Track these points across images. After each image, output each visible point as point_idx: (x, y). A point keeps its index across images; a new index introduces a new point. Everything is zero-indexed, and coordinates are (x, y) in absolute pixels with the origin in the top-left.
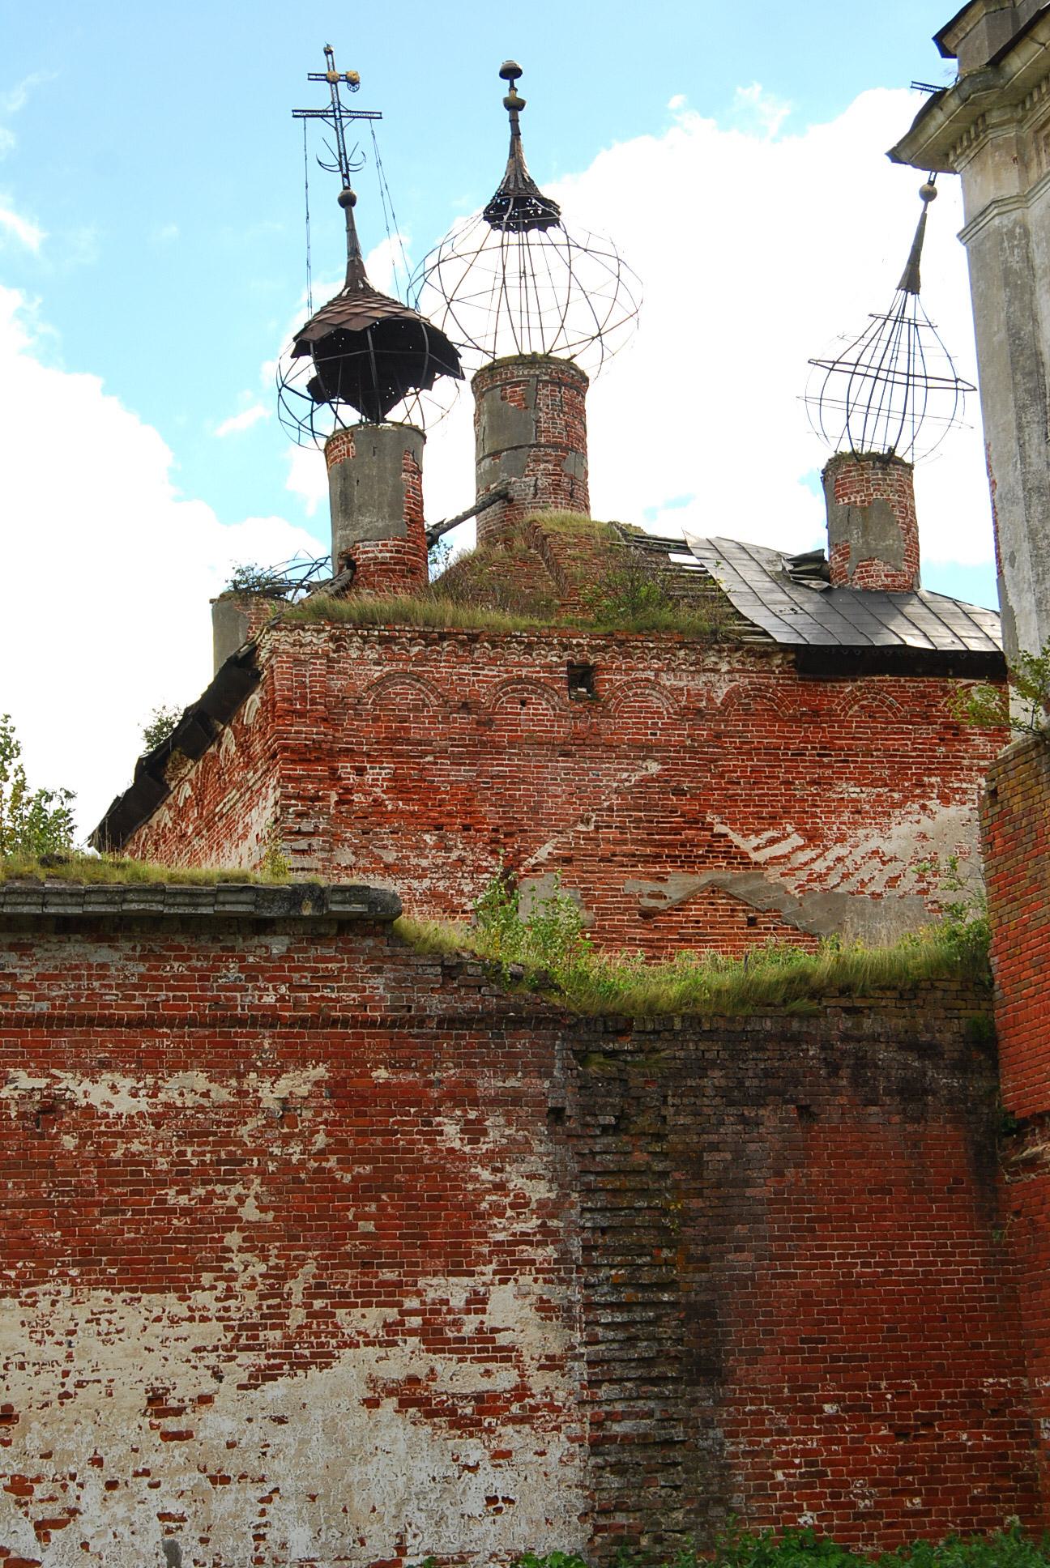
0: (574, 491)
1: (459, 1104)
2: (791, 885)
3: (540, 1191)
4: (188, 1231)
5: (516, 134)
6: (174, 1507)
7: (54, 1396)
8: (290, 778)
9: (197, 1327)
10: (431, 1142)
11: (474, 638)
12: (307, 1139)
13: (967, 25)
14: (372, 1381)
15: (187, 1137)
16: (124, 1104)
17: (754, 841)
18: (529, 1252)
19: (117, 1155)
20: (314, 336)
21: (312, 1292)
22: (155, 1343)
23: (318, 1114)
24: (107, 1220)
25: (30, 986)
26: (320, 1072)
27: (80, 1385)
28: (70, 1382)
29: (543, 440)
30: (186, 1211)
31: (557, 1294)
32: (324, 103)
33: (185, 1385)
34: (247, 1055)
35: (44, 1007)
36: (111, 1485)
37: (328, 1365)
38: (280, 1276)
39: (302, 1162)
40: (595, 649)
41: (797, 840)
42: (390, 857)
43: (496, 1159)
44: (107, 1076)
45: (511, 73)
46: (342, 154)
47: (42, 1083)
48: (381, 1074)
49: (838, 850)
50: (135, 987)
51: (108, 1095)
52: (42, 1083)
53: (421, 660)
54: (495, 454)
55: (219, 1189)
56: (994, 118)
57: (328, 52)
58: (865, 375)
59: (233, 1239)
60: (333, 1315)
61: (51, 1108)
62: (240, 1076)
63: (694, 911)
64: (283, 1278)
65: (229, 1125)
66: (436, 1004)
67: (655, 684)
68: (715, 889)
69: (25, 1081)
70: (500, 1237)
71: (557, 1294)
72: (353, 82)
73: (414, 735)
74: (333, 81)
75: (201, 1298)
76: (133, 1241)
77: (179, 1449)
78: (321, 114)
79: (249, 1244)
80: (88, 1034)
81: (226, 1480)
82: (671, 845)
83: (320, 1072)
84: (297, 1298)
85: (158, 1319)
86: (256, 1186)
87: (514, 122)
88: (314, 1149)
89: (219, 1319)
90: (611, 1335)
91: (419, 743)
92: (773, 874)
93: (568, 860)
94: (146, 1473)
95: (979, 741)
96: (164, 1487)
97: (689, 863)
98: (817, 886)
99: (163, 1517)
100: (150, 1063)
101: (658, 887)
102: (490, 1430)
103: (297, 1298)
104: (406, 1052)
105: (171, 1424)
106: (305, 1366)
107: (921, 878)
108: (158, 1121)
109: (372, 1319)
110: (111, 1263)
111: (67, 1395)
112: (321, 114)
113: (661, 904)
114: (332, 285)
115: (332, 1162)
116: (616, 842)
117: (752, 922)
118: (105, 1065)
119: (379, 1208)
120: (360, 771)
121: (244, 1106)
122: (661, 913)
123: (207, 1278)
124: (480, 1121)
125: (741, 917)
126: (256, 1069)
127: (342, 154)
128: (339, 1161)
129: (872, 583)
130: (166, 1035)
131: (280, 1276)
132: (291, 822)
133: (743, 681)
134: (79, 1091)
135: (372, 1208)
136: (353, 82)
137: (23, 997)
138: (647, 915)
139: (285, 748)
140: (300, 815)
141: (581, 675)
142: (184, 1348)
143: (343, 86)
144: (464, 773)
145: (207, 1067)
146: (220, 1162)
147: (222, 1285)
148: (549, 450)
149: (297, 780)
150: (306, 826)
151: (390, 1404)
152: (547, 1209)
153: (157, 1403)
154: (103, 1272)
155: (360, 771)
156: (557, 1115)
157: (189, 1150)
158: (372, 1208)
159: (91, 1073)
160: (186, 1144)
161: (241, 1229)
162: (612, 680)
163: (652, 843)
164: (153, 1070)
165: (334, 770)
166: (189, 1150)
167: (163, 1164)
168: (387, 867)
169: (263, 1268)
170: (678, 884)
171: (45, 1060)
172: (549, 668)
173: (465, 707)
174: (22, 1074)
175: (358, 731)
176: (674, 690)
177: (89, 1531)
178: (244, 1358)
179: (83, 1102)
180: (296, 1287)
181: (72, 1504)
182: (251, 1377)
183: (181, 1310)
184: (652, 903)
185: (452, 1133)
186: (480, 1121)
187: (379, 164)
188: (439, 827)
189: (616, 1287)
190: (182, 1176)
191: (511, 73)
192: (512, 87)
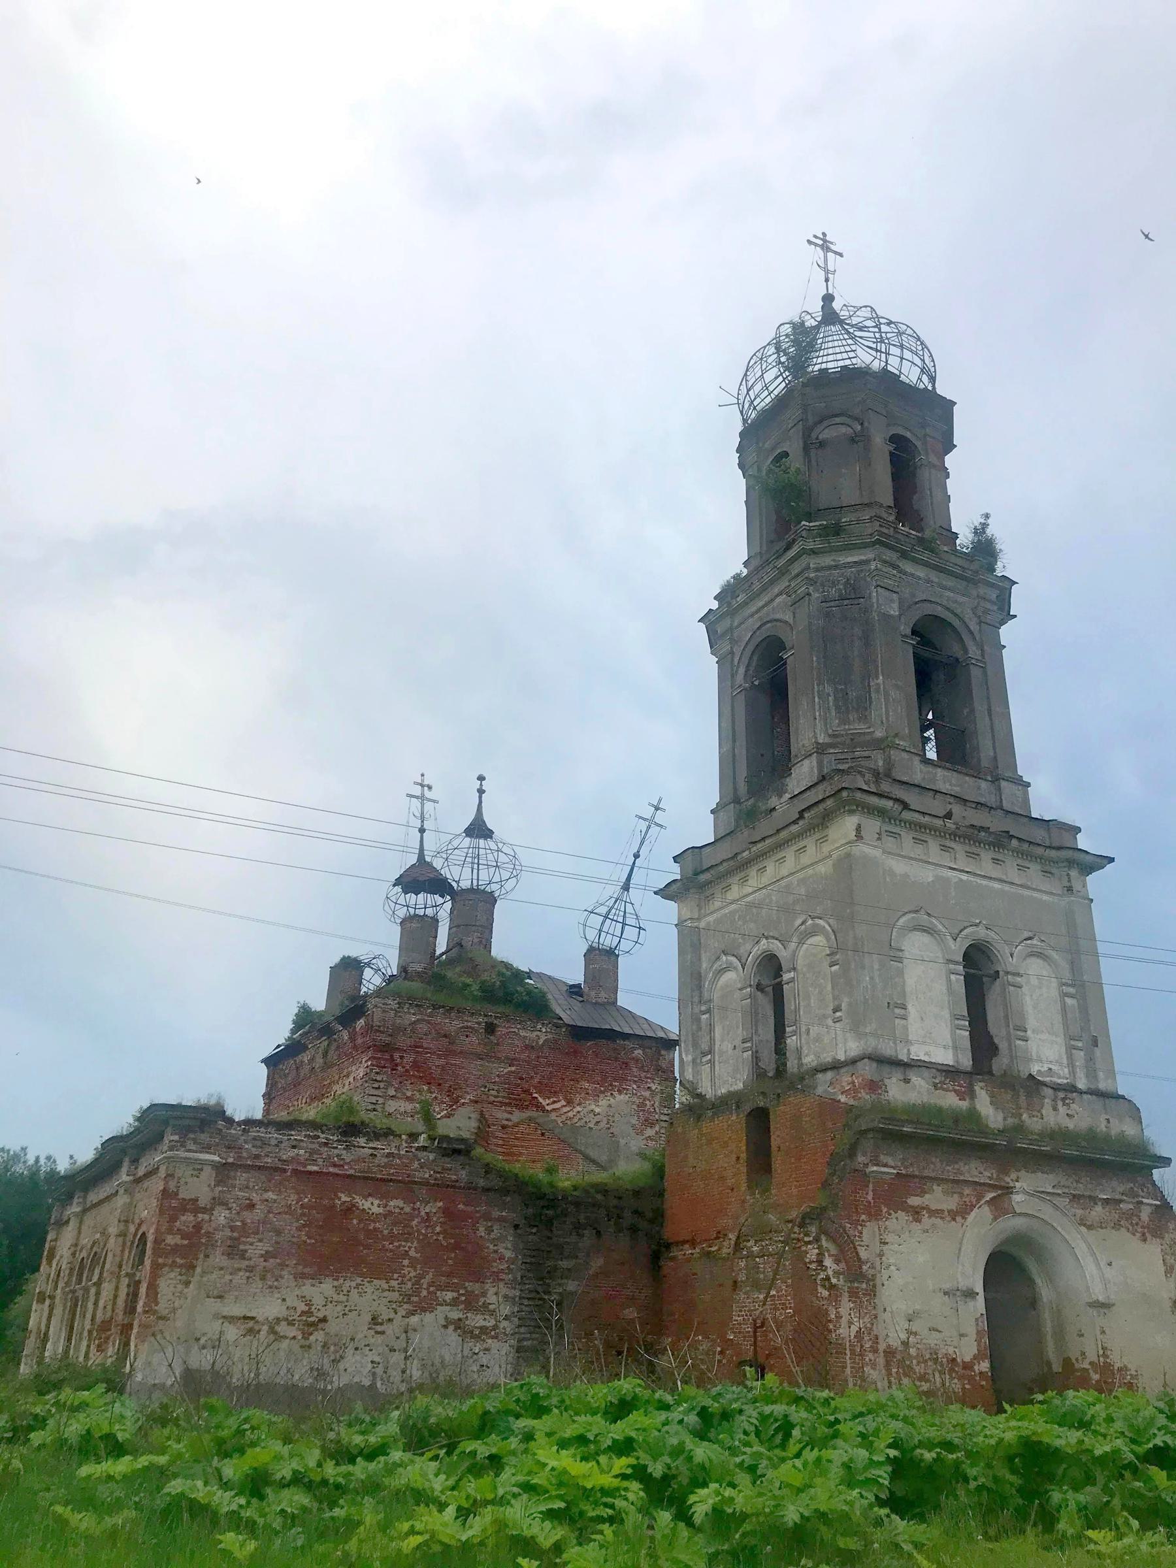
0: (488, 946)
1: (486, 1220)
2: (559, 1120)
3: (508, 1254)
5: (480, 802)
6: (377, 1359)
8: (374, 1058)
9: (390, 1293)
11: (452, 1008)
13: (685, 855)
14: (446, 1318)
15: (394, 1224)
16: (375, 1210)
17: (548, 1101)
18: (503, 1276)
19: (371, 1228)
20: (404, 880)
21: (430, 1285)
23: (439, 1218)
25: (348, 1163)
27: (350, 1311)
28: (347, 1309)
30: (391, 1251)
31: (511, 1293)
32: (418, 793)
33: (386, 1314)
35: (351, 1172)
36: (356, 1349)
38: (420, 1277)
40: (496, 1017)
41: (563, 1103)
42: (409, 1094)
43: (495, 1241)
44: (370, 1199)
45: (481, 778)
46: (422, 813)
48: (461, 1206)
49: (578, 1109)
50: (383, 1167)
51: (370, 1206)
52: (348, 1199)
54: (458, 926)
55: (403, 1243)
56: (691, 891)
57: (423, 775)
59: (406, 1262)
61: (350, 1209)
63: (521, 1128)
64: (421, 1278)
66: (482, 1183)
68: (530, 1119)
69: (344, 1198)
70: (495, 1270)
71: (511, 1293)
72: (430, 788)
73: (425, 1045)
74: (422, 786)
75: (394, 1283)
77: (380, 1338)
78: (417, 797)
79: (412, 1265)
81: (395, 1351)
82: (515, 1099)
84: (425, 1286)
86: (415, 1244)
87: (480, 797)
90: (527, 1309)
92: (553, 1116)
93: (476, 1102)
94: (368, 1345)
95: (635, 1070)
97: (521, 1107)
98: (569, 1122)
99: (372, 1362)
100: (385, 1197)
101: (509, 1116)
102: (484, 1340)
103: (425, 1286)
105: (379, 1328)
106: (425, 1311)
107: (608, 1123)
108: (385, 1216)
109: (449, 1296)
110: (365, 1267)
112: (417, 797)
113: (510, 1124)
114: (413, 859)
115: (441, 1237)
116: (496, 1097)
117: (543, 1134)
118: (370, 1195)
120: (402, 1057)
122: (509, 1127)
123: (396, 1276)
124: (491, 1226)
125: (539, 1132)
127: (422, 813)
129: (599, 1000)
131: (420, 1277)
132: (373, 1076)
133: (550, 1036)
135: (453, 1255)
136: (430, 788)
137: (346, 1167)
138: (504, 1127)
139: (375, 1046)
140: (377, 1073)
141: (490, 1029)
143: (426, 788)
144: (442, 1062)
150: (379, 1078)
151: (451, 1328)
152: (512, 1261)
153: (375, 1320)
155: (402, 1057)
156: (516, 1227)
158: (453, 1255)
159: (365, 1197)
162: (501, 1031)
163: (510, 1098)
165: (392, 1056)
167: (386, 1232)
168: (407, 1097)
169: (414, 1274)
170: (517, 1116)
172: (479, 1023)
173: (445, 1036)
174: (343, 1195)
175: (403, 1041)
176: (525, 1037)
177: (347, 1366)
178: (405, 1306)
179: (361, 1208)
183: (386, 1286)
184: (506, 1123)
185: (482, 1231)
186: (491, 1226)
187: (436, 819)
188: (429, 1084)
189: (530, 1291)
190: (392, 1238)
191: (481, 778)
192: (481, 785)
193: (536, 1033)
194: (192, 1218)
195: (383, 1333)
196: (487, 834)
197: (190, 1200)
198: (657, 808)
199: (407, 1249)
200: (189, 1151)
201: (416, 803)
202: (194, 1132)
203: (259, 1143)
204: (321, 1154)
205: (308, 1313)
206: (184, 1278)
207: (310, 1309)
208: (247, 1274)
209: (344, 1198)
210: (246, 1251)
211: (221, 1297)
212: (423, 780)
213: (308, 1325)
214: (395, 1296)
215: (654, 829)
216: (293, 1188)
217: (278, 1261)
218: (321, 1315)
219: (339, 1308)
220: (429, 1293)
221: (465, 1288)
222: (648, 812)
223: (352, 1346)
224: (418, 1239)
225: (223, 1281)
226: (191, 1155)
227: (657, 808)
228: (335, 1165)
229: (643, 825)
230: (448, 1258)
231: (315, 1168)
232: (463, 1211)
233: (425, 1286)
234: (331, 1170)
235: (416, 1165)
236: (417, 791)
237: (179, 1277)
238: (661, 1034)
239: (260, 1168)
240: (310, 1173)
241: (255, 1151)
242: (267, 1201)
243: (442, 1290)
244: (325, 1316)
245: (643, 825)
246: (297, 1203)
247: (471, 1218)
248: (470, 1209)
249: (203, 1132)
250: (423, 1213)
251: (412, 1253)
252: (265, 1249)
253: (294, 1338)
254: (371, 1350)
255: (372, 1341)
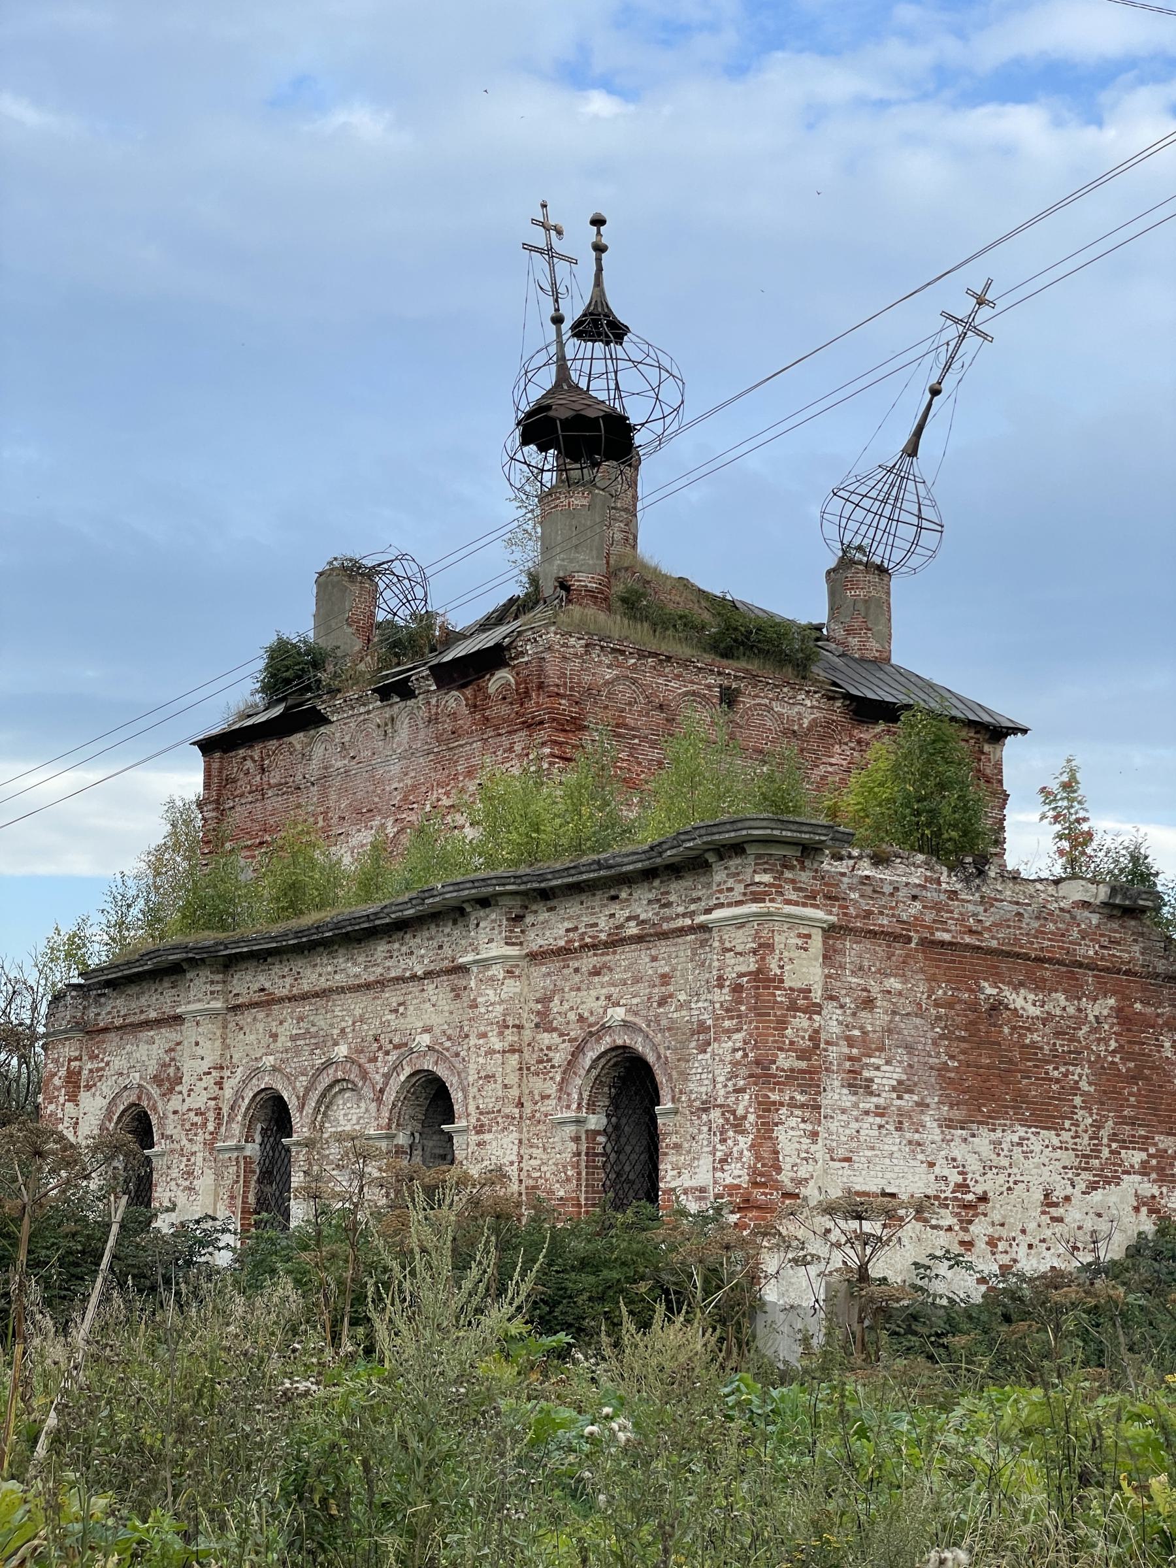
4: (1059, 1093)
5: (600, 269)
7: (1004, 1189)
10: (1159, 1052)
12: (1106, 1041)
15: (1057, 1034)
19: (1027, 1041)
21: (1113, 1138)
22: (1046, 1161)
23: (1111, 1028)
24: (1025, 1081)
25: (989, 929)
26: (1112, 1002)
27: (1015, 1183)
28: (1011, 1180)
29: (619, 505)
30: (1058, 1081)
32: (542, 244)
34: (1082, 986)
35: (994, 944)
37: (1118, 1184)
38: (1098, 1126)
39: (1105, 1057)
46: (554, 285)
47: (995, 991)
51: (1023, 1002)
52: (995, 991)
53: (634, 668)
55: (1071, 1068)
57: (544, 206)
58: (847, 500)
59: (1078, 1100)
60: (1119, 1153)
61: (997, 1007)
62: (1080, 999)
64: (1099, 1128)
65: (1074, 1029)
67: (770, 709)
69: (990, 991)
73: (632, 723)
75: (1066, 1136)
76: (1035, 1097)
80: (1013, 963)
83: (1112, 1002)
85: (1047, 1147)
87: (599, 260)
88: (1111, 1049)
89: (1073, 1150)
91: (633, 729)
94: (1043, 1241)
96: (1052, 1250)
100: (1040, 986)
104: (1148, 994)
106: (1109, 1183)
109: (1136, 1157)
110: (1027, 1109)
111: (1009, 1189)
114: (547, 379)
118: (1022, 984)
119: (1139, 1090)
121: (1080, 1019)
126: (1086, 996)
127: (554, 285)
128: (1121, 1059)
130: (1046, 969)
131: (1098, 1126)
133: (817, 714)
134: (1011, 998)
136: (559, 233)
142: (1059, 1165)
143: (553, 233)
145: (1065, 991)
146: (1070, 1052)
147: (1073, 1128)
148: (622, 513)
149: (560, 744)
151: (1144, 1210)
153: (1048, 1202)
154: (1023, 1114)
157: (1058, 1042)
158: (1135, 1089)
160: (1058, 1038)
161: (1081, 1095)
162: (746, 701)
164: (1042, 989)
166: (1058, 1042)
171: (997, 978)
172: (709, 687)
173: (661, 707)
174: (986, 984)
176: (781, 715)
180: (1104, 1133)
181: (1014, 1256)
182: (1087, 1187)
183: (1056, 1142)
190: (1056, 1058)
192: (599, 233)
193: (797, 709)
194: (805, 1023)
195: (1060, 1220)
196: (616, 332)
197: (801, 991)
198: (981, 302)
199: (1076, 1078)
200: (788, 902)
201: (540, 261)
202: (792, 868)
203: (868, 890)
204: (952, 912)
205: (963, 1187)
206: (809, 1127)
207: (965, 1180)
208: (878, 1120)
209: (990, 991)
210: (871, 1080)
211: (848, 1160)
212: (546, 216)
213: (965, 1207)
214: (1068, 1158)
215: (972, 340)
216: (922, 970)
217: (916, 1098)
218: (979, 1190)
219: (1001, 1179)
220: (1111, 1152)
221: (1155, 1145)
222: (964, 307)
223: (1023, 1240)
224: (1089, 1061)
225: (848, 1132)
226: (789, 909)
227: (981, 302)
228: (971, 932)
229: (953, 331)
230: (1129, 1094)
231: (947, 937)
232: (1140, 1014)
233: (1105, 1141)
234: (968, 939)
235: (1075, 934)
236: (538, 238)
237: (802, 1126)
238: (986, 718)
239: (874, 934)
240: (942, 944)
241: (865, 905)
242: (889, 992)
243: (1127, 1148)
244: (985, 1193)
245: (953, 331)
246: (929, 997)
247: (1153, 1027)
248: (1149, 1010)
249: (803, 869)
250: (1091, 1018)
251: (1084, 1085)
252: (895, 1076)
253: (950, 1229)
254: (1048, 1249)
255: (1048, 1233)
